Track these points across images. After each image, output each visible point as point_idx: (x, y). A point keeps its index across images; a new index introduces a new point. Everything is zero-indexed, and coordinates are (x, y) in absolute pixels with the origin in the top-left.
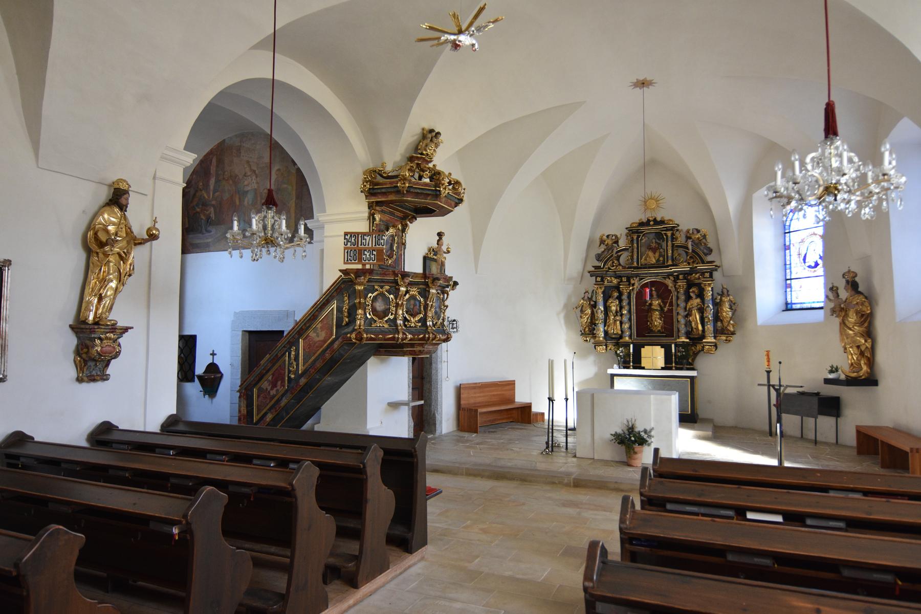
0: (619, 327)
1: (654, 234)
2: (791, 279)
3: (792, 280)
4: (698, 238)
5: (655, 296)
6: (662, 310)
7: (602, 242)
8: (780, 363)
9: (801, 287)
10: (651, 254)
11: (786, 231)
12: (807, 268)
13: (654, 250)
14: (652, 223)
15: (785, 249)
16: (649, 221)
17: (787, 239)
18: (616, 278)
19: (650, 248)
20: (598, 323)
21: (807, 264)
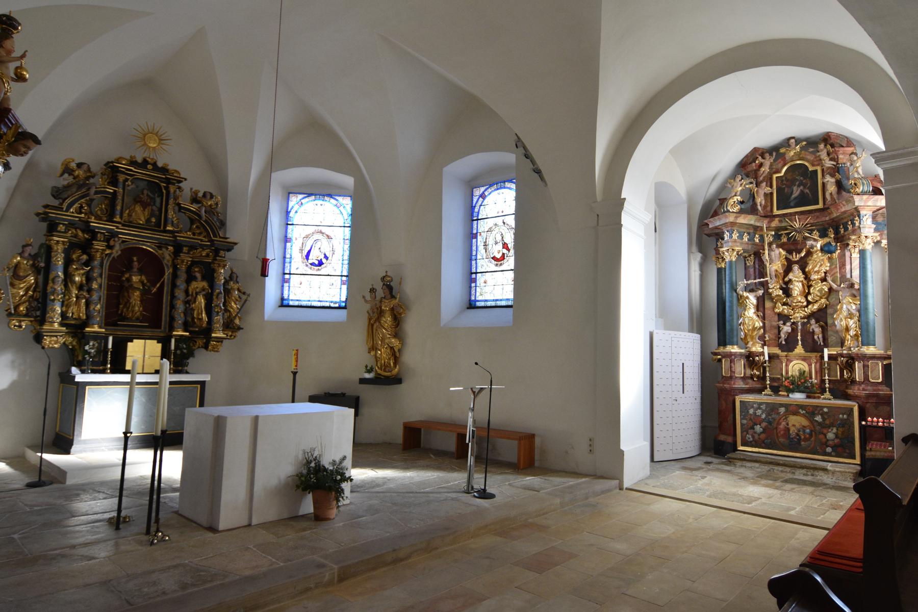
0: (83, 308)
1: (146, 183)
2: (476, 273)
3: (340, 275)
4: (211, 205)
5: (135, 270)
6: (145, 292)
7: (67, 170)
8: (476, 364)
9: (301, 284)
10: (138, 208)
11: (474, 219)
12: (310, 266)
13: (144, 206)
14: (150, 167)
15: (473, 238)
16: (145, 162)
17: (475, 226)
18: (83, 232)
19: (137, 200)
20: (53, 300)
21: (310, 261)
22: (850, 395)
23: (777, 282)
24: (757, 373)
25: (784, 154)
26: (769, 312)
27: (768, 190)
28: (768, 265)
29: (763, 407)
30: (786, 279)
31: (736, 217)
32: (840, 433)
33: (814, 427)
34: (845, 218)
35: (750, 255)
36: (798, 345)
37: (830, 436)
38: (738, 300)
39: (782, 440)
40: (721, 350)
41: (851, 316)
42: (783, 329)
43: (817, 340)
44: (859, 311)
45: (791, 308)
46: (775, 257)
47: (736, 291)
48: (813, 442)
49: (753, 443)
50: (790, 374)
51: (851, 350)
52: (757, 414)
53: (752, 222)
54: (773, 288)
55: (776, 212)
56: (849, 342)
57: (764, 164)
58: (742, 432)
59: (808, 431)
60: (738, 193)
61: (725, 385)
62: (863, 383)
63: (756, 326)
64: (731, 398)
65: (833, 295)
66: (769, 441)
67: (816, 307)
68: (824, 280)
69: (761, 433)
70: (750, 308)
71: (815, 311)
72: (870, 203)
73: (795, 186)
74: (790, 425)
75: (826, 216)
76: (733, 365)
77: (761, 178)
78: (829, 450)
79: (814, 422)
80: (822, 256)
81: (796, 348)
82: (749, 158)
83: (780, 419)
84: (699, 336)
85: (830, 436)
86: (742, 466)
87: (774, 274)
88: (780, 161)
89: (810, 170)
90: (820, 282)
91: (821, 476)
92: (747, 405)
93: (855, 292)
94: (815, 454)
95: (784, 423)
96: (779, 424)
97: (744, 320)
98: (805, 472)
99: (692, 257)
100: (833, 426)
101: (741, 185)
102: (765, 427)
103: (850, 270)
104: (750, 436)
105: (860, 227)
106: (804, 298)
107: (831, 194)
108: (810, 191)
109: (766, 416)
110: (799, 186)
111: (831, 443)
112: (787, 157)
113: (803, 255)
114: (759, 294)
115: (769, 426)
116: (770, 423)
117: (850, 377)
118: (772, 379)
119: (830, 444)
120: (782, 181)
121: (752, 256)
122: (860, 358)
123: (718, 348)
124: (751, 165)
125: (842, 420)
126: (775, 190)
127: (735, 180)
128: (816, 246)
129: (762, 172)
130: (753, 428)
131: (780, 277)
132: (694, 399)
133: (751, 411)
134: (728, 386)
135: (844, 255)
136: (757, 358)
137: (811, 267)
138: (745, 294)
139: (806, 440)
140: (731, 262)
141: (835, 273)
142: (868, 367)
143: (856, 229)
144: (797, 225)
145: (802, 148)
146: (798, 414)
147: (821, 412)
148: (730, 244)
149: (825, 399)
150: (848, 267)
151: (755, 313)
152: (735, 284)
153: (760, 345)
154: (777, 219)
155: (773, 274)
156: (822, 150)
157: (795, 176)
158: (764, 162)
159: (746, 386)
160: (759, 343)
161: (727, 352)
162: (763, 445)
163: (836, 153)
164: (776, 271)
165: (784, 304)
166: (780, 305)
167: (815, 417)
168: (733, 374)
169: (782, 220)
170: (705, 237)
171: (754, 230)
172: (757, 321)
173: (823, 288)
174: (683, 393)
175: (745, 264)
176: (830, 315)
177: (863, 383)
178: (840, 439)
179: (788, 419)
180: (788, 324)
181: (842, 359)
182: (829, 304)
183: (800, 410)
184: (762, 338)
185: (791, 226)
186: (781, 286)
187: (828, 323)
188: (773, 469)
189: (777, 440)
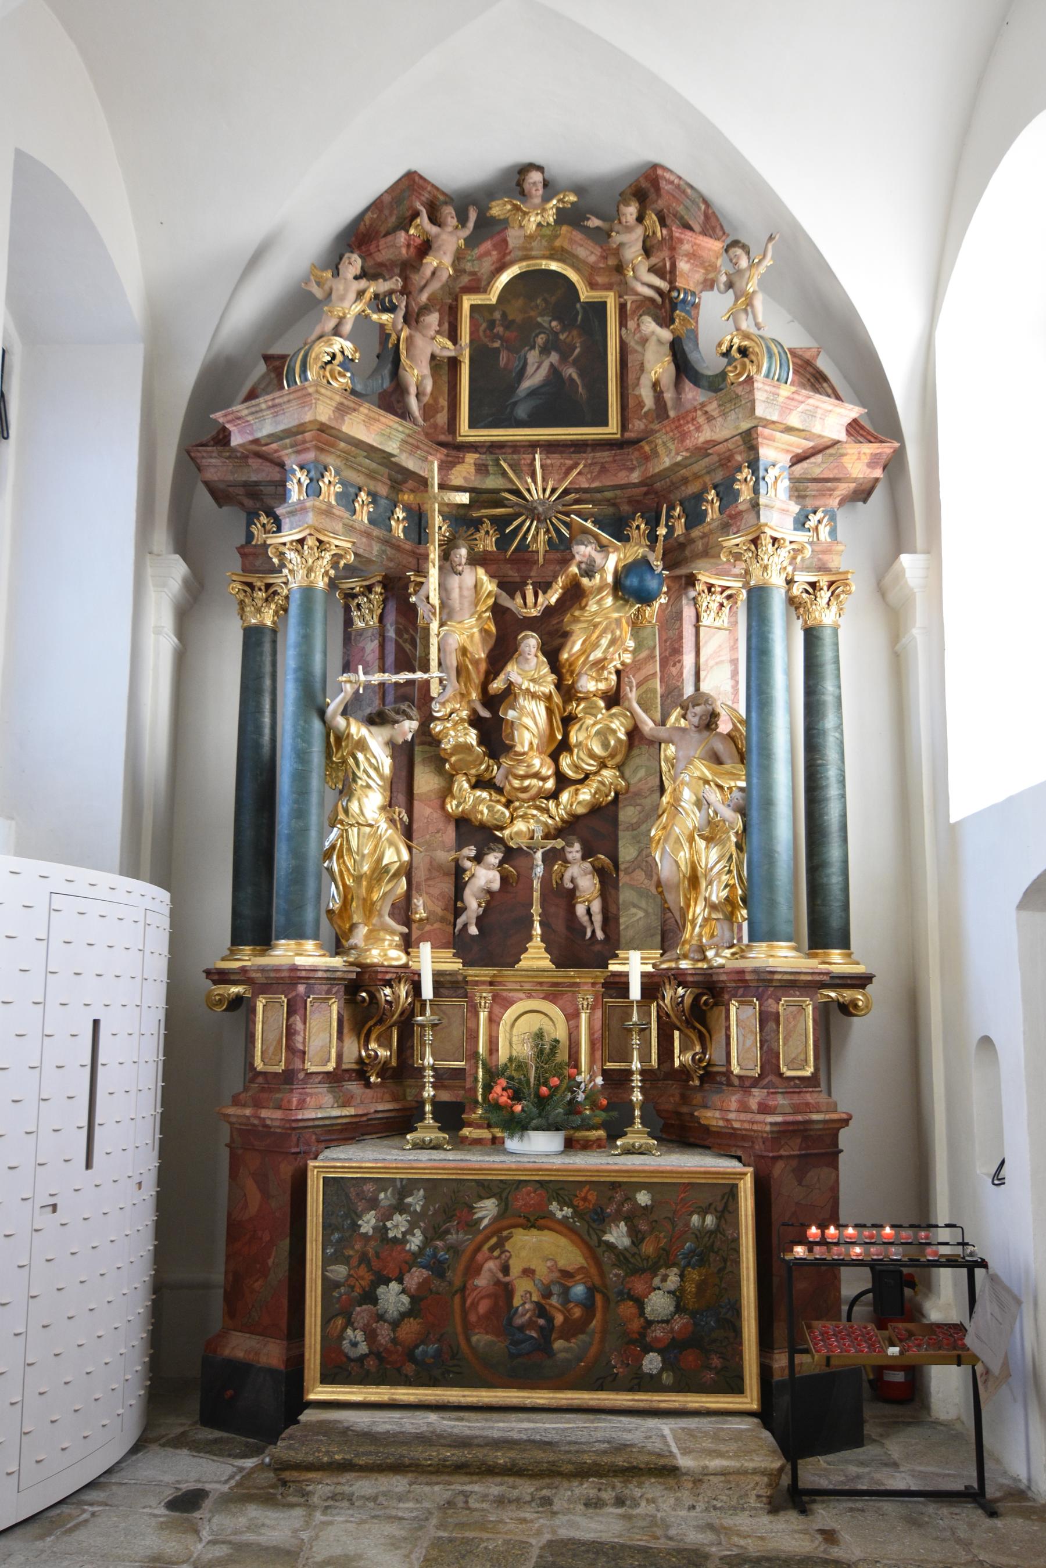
22: (706, 1129)
23: (462, 695)
24: (383, 1053)
25: (503, 224)
26: (428, 811)
27: (444, 347)
28: (434, 626)
29: (416, 1201)
30: (497, 685)
31: (342, 410)
32: (691, 1288)
33: (602, 1274)
34: (697, 476)
35: (369, 589)
36: (530, 938)
37: (659, 1303)
38: (328, 754)
39: (481, 1339)
40: (248, 959)
41: (712, 833)
42: (473, 875)
43: (584, 919)
44: (743, 811)
45: (503, 800)
46: (461, 596)
47: (322, 713)
48: (597, 1337)
49: (371, 1363)
50: (503, 1055)
51: (705, 959)
52: (391, 1234)
53: (392, 447)
54: (447, 718)
55: (465, 432)
56: (697, 930)
57: (435, 246)
58: (326, 1321)
59: (579, 1290)
60: (347, 327)
61: (264, 1113)
62: (756, 1082)
63: (385, 862)
64: (286, 1170)
65: (641, 758)
66: (432, 1348)
67: (585, 795)
68: (613, 699)
69: (404, 1315)
70: (369, 786)
71: (581, 810)
72: (794, 420)
73: (533, 347)
74: (516, 1269)
75: (632, 470)
76: (299, 1026)
77: (424, 297)
78: (652, 1363)
79: (599, 1251)
80: (618, 610)
81: (526, 950)
82: (386, 212)
83: (478, 1249)
84: (165, 896)
85: (659, 1303)
86: (334, 1497)
87: (455, 664)
88: (485, 255)
89: (583, 298)
90: (602, 704)
91: (653, 1501)
92: (353, 1195)
93: (720, 747)
94: (601, 1388)
95: (491, 1265)
96: (473, 1269)
97: (344, 836)
98: (593, 1493)
99: (149, 571)
100: (668, 1266)
101: (360, 294)
102: (420, 1285)
103: (693, 672)
104: (359, 1336)
105: (758, 505)
106: (549, 760)
107: (656, 385)
108: (580, 375)
109: (427, 1241)
110: (545, 351)
111: (658, 1333)
112: (514, 237)
113: (553, 598)
114: (405, 734)
115: (436, 1282)
116: (438, 1269)
117: (701, 1060)
118: (442, 1077)
119: (657, 1339)
120: (492, 324)
121: (378, 589)
122: (747, 987)
123: (231, 956)
124: (390, 238)
125: (701, 1234)
126: (467, 353)
127: (336, 273)
128: (602, 569)
129: (428, 272)
130: (370, 1297)
131: (474, 675)
132: (132, 1184)
133: (368, 1223)
134: (278, 1114)
135: (679, 616)
136: (388, 991)
137: (577, 647)
138: (357, 730)
139: (572, 1329)
140: (308, 591)
141: (647, 679)
142: (778, 1024)
143: (740, 513)
144: (536, 491)
145: (564, 216)
146: (542, 1222)
147: (626, 1207)
148: (311, 518)
149: (629, 1151)
150: (688, 659)
151: (383, 808)
152: (318, 686)
153: (397, 938)
154: (471, 458)
155: (452, 661)
156: (629, 229)
157: (532, 313)
158: (437, 236)
159: (346, 1112)
160: (393, 932)
161: (277, 969)
162: (410, 1369)
163: (672, 245)
164: (464, 651)
165: (480, 783)
166: (466, 785)
167: (605, 1233)
168: (298, 1065)
169: (486, 466)
170: (203, 499)
171: (392, 487)
172: (391, 843)
173: (613, 726)
174: (89, 1165)
175: (348, 622)
176: (627, 829)
177: (756, 1082)
178: (693, 1314)
179: (508, 1246)
180: (493, 858)
181: (681, 991)
182: (627, 791)
183: (554, 1207)
184: (403, 911)
185: (517, 493)
186: (474, 711)
187: (621, 860)
188: (466, 1495)
189: (461, 1339)
